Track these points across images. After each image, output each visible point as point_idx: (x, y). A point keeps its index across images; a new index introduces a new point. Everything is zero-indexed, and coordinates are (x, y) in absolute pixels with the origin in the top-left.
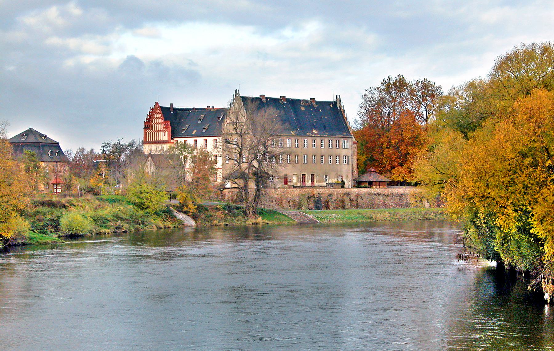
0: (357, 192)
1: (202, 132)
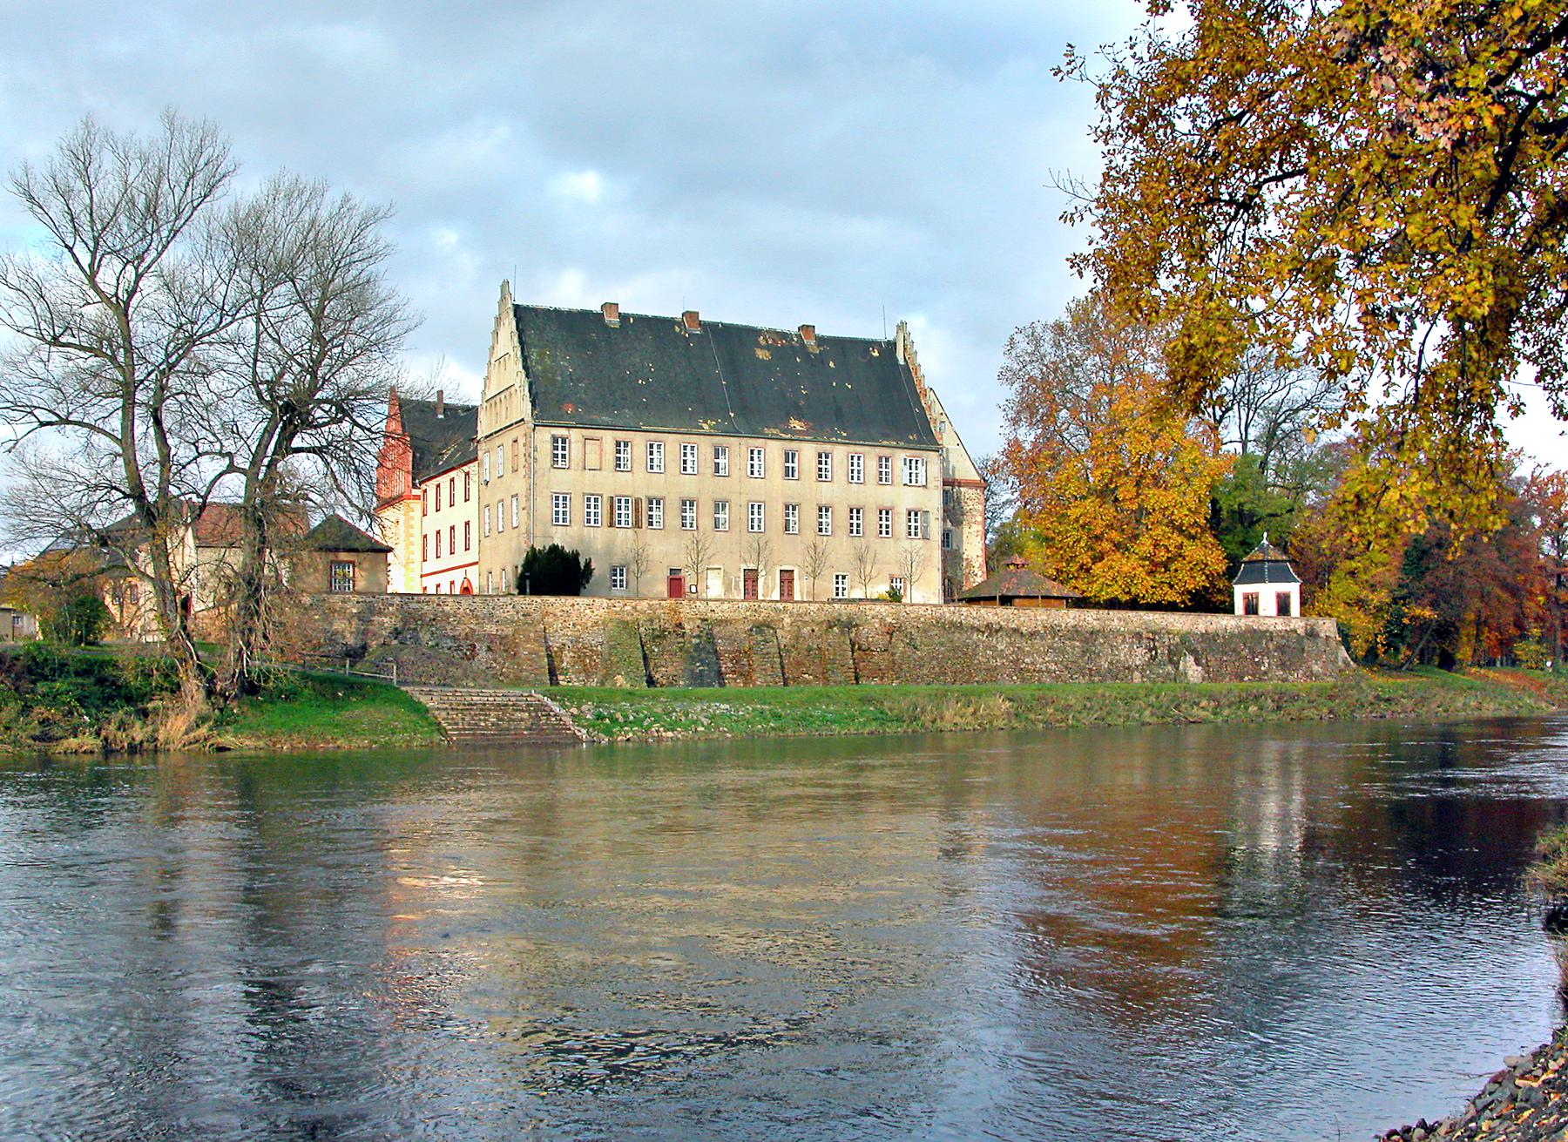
0: (889, 620)
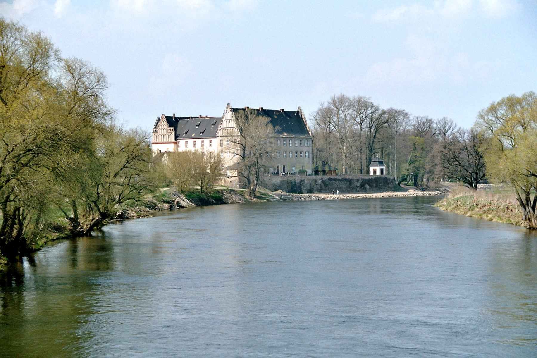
1: (200, 135)
